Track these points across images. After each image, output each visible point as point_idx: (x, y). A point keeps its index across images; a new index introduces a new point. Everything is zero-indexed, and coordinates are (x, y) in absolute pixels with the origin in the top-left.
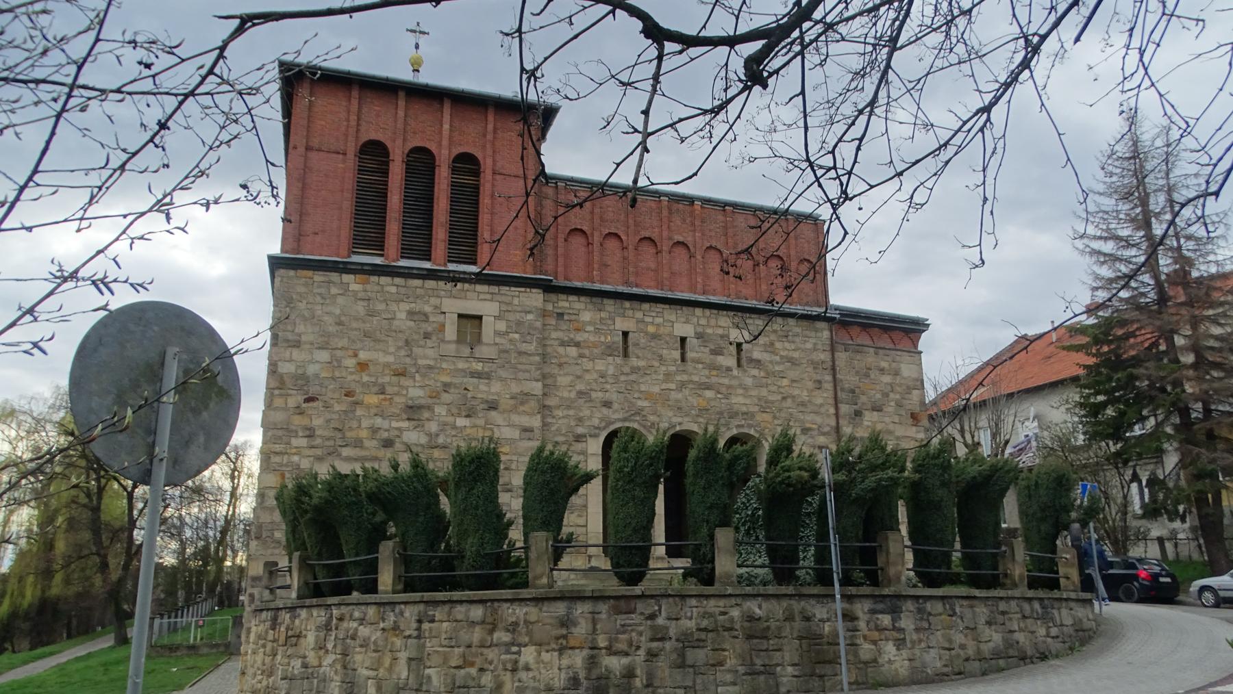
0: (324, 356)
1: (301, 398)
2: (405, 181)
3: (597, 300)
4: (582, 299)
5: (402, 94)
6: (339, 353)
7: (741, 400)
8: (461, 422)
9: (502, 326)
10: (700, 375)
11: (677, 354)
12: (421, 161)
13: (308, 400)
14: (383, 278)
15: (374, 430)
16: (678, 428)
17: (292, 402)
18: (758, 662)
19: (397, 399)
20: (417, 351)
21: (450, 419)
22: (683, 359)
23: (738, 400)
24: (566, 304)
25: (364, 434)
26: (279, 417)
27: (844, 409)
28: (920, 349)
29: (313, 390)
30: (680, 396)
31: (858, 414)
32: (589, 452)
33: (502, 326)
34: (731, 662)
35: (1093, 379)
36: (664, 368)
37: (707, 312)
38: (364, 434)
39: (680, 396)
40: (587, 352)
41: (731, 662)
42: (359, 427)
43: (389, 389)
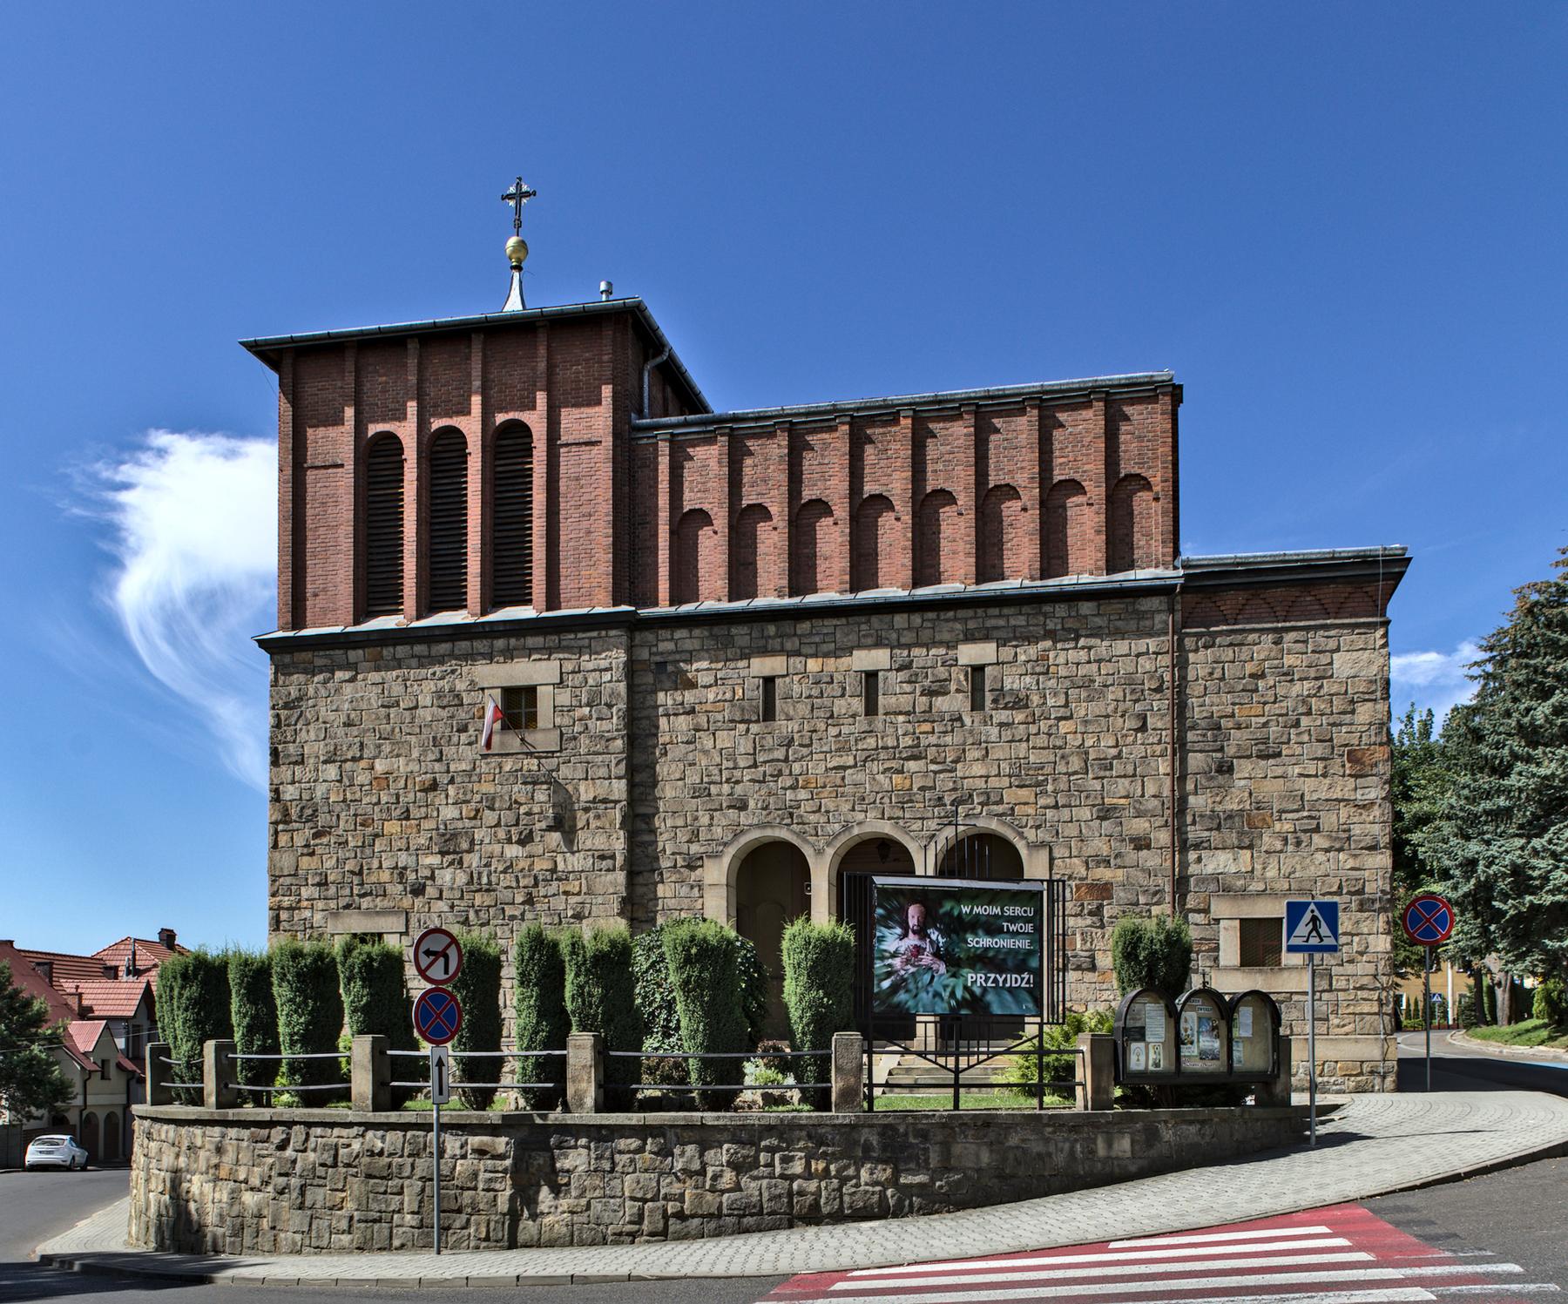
0: (332, 771)
1: (308, 833)
2: (447, 466)
3: (719, 630)
4: (697, 632)
5: (412, 346)
6: (348, 766)
7: (978, 769)
8: (513, 851)
9: (564, 698)
10: (898, 732)
11: (858, 705)
12: (443, 453)
13: (317, 835)
14: (399, 648)
15: (401, 872)
16: (856, 831)
17: (299, 840)
18: (374, 1206)
19: (426, 825)
20: (449, 751)
21: (497, 848)
22: (871, 709)
23: (974, 770)
24: (670, 646)
25: (385, 876)
26: (286, 861)
27: (1196, 761)
28: (1389, 614)
29: (323, 820)
30: (860, 777)
31: (1226, 769)
32: (707, 881)
33: (564, 698)
34: (350, 1205)
35: (62, 1082)
36: (833, 731)
37: (916, 619)
38: (385, 876)
39: (860, 777)
40: (703, 720)
41: (350, 1205)
42: (380, 867)
43: (415, 813)
